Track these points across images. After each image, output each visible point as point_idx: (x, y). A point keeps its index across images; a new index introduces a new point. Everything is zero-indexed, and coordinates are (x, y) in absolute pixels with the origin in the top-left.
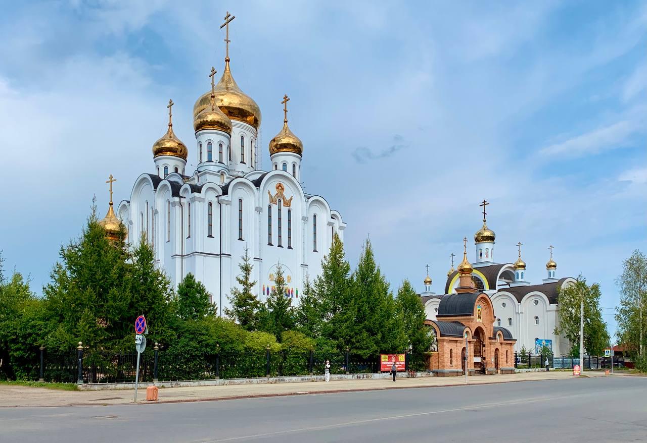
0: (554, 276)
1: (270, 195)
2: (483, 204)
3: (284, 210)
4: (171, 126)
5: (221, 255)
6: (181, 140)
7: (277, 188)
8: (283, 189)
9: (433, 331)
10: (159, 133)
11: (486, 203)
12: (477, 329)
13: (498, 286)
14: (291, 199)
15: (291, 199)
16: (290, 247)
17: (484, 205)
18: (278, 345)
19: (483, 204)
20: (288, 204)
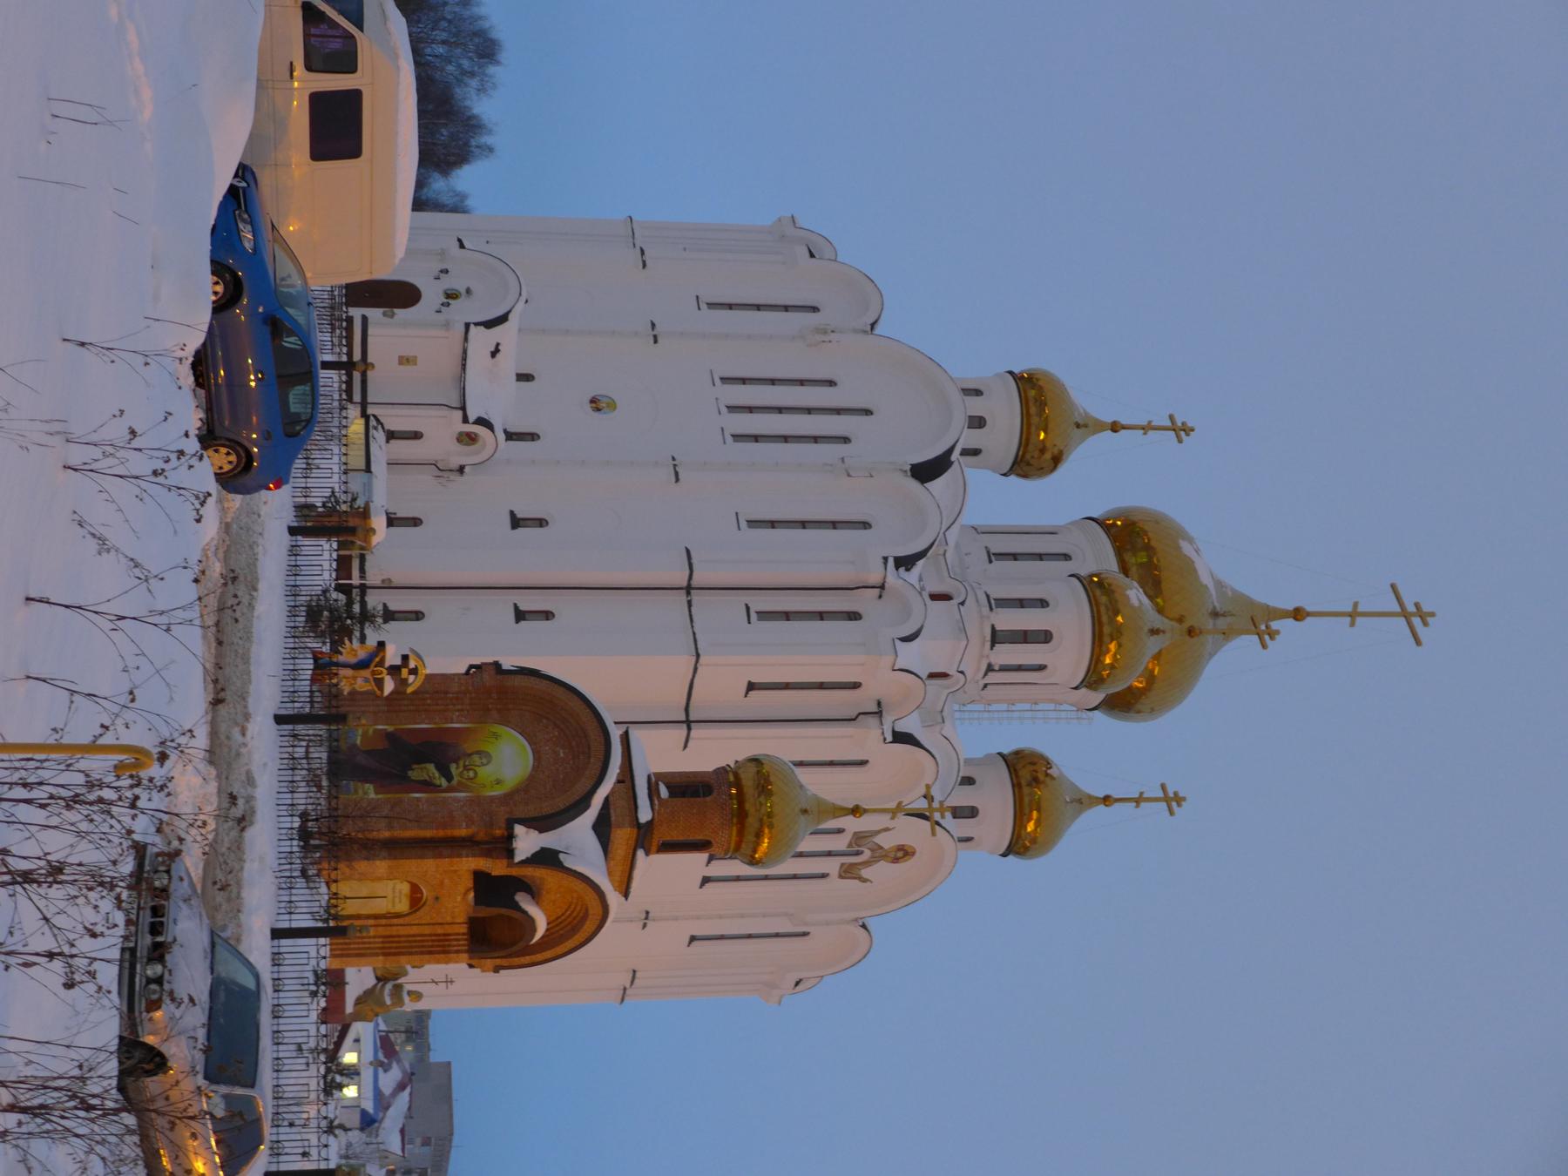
0: (362, 577)
1: (878, 832)
2: (1411, 608)
3: (832, 866)
4: (1114, 430)
5: (688, 723)
6: (1072, 457)
7: (901, 848)
8: (896, 860)
9: (287, 1079)
10: (1087, 392)
11: (1416, 621)
12: (160, 1055)
13: (365, 319)
14: (865, 881)
15: (865, 881)
16: (706, 880)
17: (1405, 614)
18: (372, 796)
19: (1411, 608)
20: (848, 872)
